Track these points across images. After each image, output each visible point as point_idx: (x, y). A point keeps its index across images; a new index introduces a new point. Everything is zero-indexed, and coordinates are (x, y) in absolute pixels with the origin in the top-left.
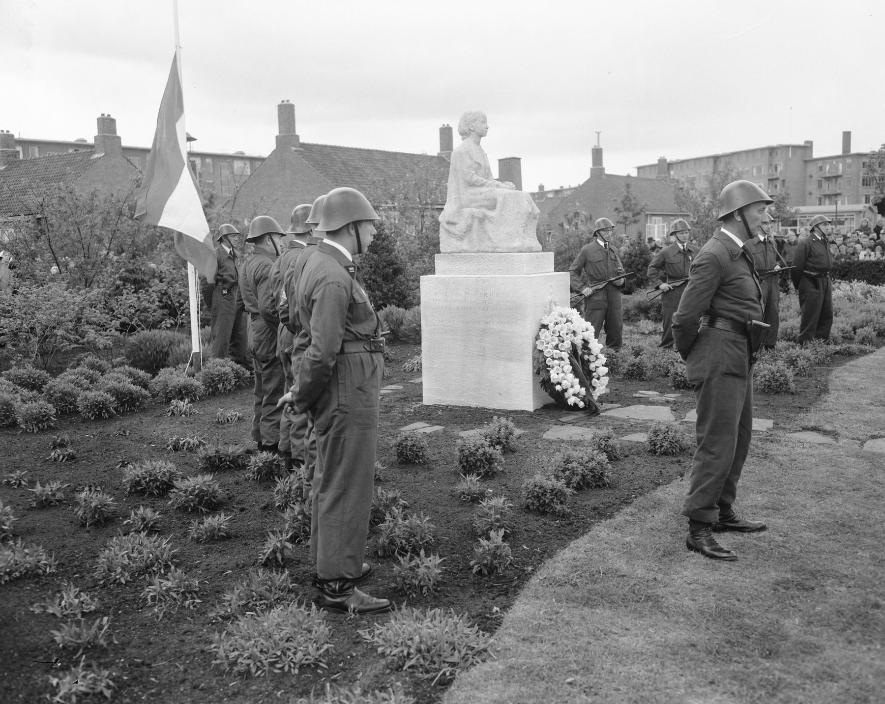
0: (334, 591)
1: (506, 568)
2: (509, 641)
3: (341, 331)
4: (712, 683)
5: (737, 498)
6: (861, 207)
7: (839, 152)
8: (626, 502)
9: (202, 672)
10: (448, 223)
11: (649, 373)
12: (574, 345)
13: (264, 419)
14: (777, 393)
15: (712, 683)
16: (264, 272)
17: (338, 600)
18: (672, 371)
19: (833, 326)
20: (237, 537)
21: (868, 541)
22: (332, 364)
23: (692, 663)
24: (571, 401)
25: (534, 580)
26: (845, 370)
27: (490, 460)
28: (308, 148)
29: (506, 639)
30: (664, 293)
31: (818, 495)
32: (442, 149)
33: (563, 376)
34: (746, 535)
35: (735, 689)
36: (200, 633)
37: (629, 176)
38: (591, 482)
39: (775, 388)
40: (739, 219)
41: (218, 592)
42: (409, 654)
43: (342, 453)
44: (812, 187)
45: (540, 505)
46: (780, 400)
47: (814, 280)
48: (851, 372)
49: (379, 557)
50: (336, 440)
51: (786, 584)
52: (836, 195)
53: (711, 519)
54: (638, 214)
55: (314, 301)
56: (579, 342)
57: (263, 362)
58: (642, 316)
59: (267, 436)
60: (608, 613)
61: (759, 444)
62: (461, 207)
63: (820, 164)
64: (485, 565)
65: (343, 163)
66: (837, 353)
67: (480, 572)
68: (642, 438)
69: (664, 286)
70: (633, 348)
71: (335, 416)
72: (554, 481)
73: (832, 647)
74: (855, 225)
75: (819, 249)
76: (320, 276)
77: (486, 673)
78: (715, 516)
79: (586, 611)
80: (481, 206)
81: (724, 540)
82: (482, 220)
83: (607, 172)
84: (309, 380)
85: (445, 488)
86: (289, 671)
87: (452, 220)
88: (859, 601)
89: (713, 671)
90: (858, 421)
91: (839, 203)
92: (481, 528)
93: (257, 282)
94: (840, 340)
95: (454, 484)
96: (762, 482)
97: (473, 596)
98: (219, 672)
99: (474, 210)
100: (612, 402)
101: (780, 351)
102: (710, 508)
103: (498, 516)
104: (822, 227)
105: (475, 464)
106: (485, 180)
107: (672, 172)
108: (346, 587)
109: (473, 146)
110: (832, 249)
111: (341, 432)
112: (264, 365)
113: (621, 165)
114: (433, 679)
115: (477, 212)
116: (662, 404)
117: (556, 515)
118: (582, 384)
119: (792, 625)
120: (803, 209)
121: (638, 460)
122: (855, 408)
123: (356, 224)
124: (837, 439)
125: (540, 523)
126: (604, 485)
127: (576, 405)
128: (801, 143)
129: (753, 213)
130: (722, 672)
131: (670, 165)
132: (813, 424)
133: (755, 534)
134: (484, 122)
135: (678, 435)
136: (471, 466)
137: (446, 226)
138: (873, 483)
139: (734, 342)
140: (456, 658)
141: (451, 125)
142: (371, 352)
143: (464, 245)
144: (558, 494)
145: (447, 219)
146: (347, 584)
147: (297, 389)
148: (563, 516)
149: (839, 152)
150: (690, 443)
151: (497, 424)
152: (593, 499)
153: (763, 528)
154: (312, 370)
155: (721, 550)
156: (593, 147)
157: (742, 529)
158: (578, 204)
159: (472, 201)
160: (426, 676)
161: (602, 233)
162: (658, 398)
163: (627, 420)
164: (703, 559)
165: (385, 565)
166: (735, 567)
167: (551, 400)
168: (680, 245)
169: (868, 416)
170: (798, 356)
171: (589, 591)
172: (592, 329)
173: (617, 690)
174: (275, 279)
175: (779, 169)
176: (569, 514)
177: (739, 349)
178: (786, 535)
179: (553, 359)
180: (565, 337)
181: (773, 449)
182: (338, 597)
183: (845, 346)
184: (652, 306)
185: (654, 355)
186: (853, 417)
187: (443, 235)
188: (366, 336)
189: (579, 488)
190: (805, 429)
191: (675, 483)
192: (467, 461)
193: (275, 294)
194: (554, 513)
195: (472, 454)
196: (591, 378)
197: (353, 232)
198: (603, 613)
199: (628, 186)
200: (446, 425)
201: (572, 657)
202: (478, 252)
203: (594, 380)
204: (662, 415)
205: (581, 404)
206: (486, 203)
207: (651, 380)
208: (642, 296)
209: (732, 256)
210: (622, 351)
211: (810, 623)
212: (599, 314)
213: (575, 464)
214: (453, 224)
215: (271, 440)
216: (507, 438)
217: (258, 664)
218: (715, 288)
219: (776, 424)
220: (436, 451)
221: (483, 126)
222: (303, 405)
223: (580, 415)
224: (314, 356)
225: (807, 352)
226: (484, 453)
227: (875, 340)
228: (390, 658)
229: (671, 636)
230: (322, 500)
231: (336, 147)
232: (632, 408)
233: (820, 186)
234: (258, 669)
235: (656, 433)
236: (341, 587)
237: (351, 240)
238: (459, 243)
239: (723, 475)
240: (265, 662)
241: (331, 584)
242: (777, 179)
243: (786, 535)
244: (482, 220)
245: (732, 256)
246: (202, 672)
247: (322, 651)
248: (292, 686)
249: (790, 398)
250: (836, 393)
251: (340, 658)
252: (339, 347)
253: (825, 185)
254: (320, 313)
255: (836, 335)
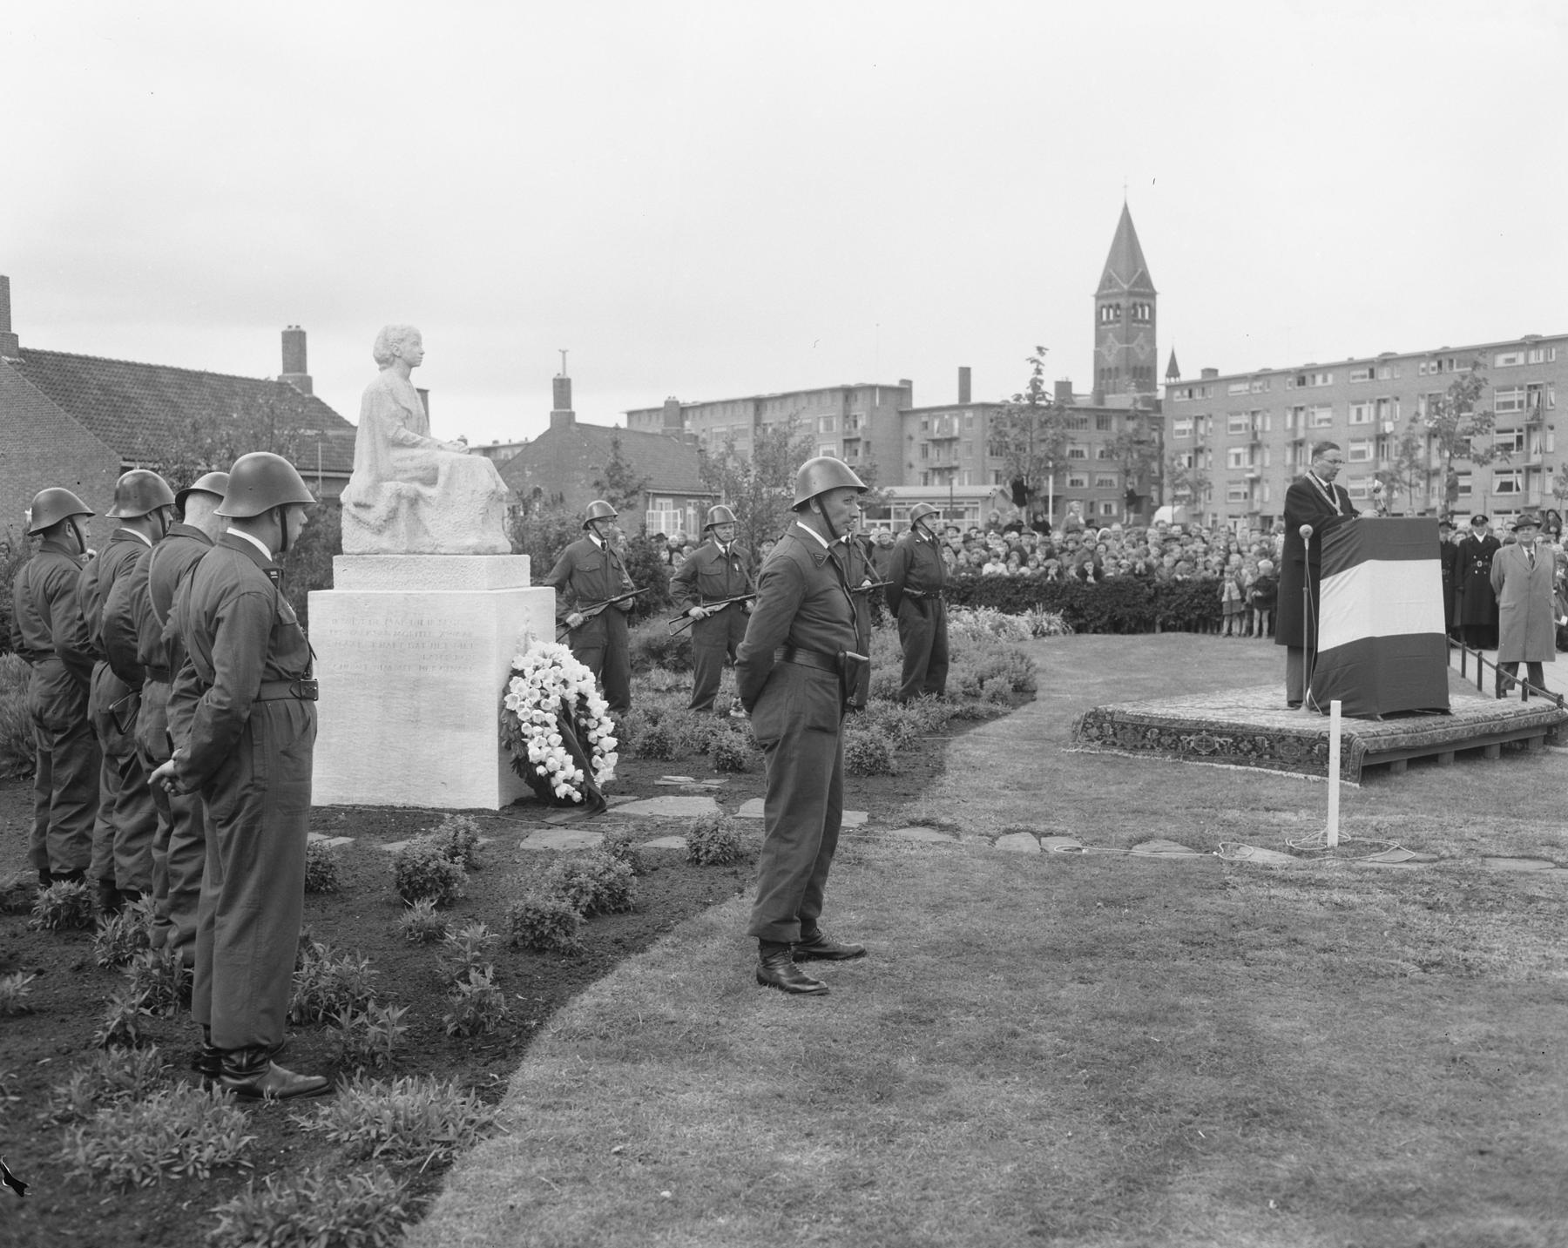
0: (239, 1068)
1: (498, 1024)
2: (522, 1110)
3: (261, 666)
4: (808, 1135)
5: (825, 908)
6: (986, 490)
7: (955, 401)
8: (664, 929)
9: (49, 1191)
10: (357, 505)
11: (676, 750)
12: (564, 702)
13: (54, 830)
14: (871, 774)
15: (808, 1135)
16: (63, 581)
17: (246, 1081)
18: (714, 743)
19: (949, 676)
20: (41, 1011)
21: (1003, 961)
22: (246, 715)
23: (780, 1117)
24: (561, 791)
25: (546, 1036)
26: (968, 740)
27: (446, 880)
28: (34, 360)
29: (518, 1108)
30: (698, 623)
31: (935, 908)
32: (286, 370)
33: (548, 751)
34: (839, 963)
35: (840, 1139)
36: (27, 1144)
37: (617, 428)
38: (608, 903)
39: (871, 767)
40: (817, 510)
41: (38, 1087)
42: (379, 1135)
43: (256, 852)
44: (913, 454)
45: (534, 937)
46: (875, 784)
47: (919, 603)
48: (976, 742)
49: (293, 1024)
50: (247, 831)
51: (897, 1018)
52: (951, 469)
53: (791, 941)
54: (634, 493)
55: (219, 620)
56: (572, 698)
57: (56, 732)
58: (653, 663)
59: (60, 858)
60: (657, 1067)
61: (850, 845)
62: (380, 479)
63: (924, 418)
64: (466, 1022)
65: (101, 387)
66: (956, 716)
67: (457, 1033)
68: (677, 843)
69: (696, 611)
70: (646, 713)
71: (247, 795)
72: (555, 902)
73: (959, 1084)
74: (980, 521)
75: (924, 555)
76: (229, 583)
77: (497, 1149)
78: (794, 932)
79: (627, 1067)
80: (413, 479)
81: (810, 970)
82: (414, 501)
83: (579, 419)
84: (207, 739)
85: (375, 924)
86: (196, 1175)
87: (363, 500)
88: (991, 1030)
89: (809, 1121)
90: (987, 811)
91: (955, 482)
92: (466, 962)
93: (50, 599)
94: (960, 697)
95: (390, 919)
96: (856, 895)
97: (453, 1064)
98: (77, 1186)
99: (401, 484)
100: (623, 793)
101: (871, 714)
102: (787, 920)
103: (477, 953)
104: (927, 522)
105: (422, 888)
106: (419, 438)
107: (687, 424)
108: (259, 1059)
109: (399, 381)
110: (947, 555)
111: (255, 819)
112: (58, 737)
113: (599, 409)
114: (420, 1165)
115: (408, 488)
116: (700, 794)
117: (559, 951)
118: (578, 764)
119: (908, 1064)
120: (900, 491)
121: (673, 873)
122: (983, 793)
123: (284, 509)
124: (958, 837)
125: (537, 964)
126: (627, 909)
127: (568, 797)
128: (894, 382)
129: (837, 503)
130: (821, 1123)
131: (684, 410)
132: (924, 816)
133: (850, 962)
134: (417, 343)
135: (732, 834)
136: (415, 891)
137: (353, 510)
138: (1009, 890)
139: (822, 683)
140: (451, 1134)
141: (303, 328)
142: (301, 698)
143: (384, 542)
144: (562, 920)
145: (356, 499)
146: (259, 1054)
147: (187, 755)
148: (571, 953)
149: (955, 401)
150: (748, 847)
151: (451, 826)
152: (614, 928)
153: (861, 953)
154: (215, 724)
155: (805, 981)
156: (554, 375)
157: (832, 956)
158: (529, 473)
159: (397, 471)
160: (410, 1162)
161: (597, 524)
162: (693, 785)
163: (651, 818)
164: (782, 996)
165: (304, 1034)
166: (826, 1002)
167: (530, 791)
168: (720, 546)
169: (1000, 804)
170: (900, 720)
171: (626, 1044)
172: (591, 677)
173: (684, 1154)
174: (90, 593)
175: (860, 423)
176: (580, 951)
177: (830, 693)
178: (893, 960)
179: (533, 724)
180: (550, 689)
181: (869, 852)
182: (246, 1076)
183: (969, 704)
184: (669, 646)
185: (680, 722)
186: (980, 806)
187: (347, 525)
188: (295, 674)
189: (590, 914)
190: (913, 823)
191: (731, 902)
192: (409, 883)
193: (88, 617)
194: (557, 950)
195: (418, 871)
196: (591, 755)
197: (277, 519)
198: (648, 1070)
199: (616, 444)
200: (357, 835)
201: (616, 1122)
202: (408, 552)
203: (596, 757)
204: (703, 808)
205: (577, 796)
206: (420, 474)
207: (680, 759)
208: (660, 627)
209: (817, 562)
210: (631, 716)
211: (930, 1060)
212: (595, 654)
213: (583, 877)
214: (366, 506)
215: (66, 863)
216: (468, 847)
217: (144, 1169)
218: (796, 609)
219: (871, 817)
220: (349, 874)
221: (416, 350)
222: (192, 780)
223: (577, 812)
224: (219, 703)
225: (914, 714)
226: (438, 869)
227: (1011, 696)
228: (349, 1146)
229: (749, 1088)
230: (221, 927)
231: (87, 358)
232: (656, 800)
233: (925, 453)
234: (144, 1176)
235: (698, 831)
236: (250, 1062)
237: (273, 531)
238: (375, 539)
239: (805, 871)
240: (155, 1166)
241: (233, 1057)
242: (858, 440)
243: (893, 960)
244: (414, 501)
245: (817, 562)
246: (49, 1191)
247: (242, 1144)
248: (204, 1194)
249: (890, 781)
250: (957, 773)
251: (270, 1154)
252: (256, 689)
253: (933, 452)
254: (229, 638)
255: (954, 689)
